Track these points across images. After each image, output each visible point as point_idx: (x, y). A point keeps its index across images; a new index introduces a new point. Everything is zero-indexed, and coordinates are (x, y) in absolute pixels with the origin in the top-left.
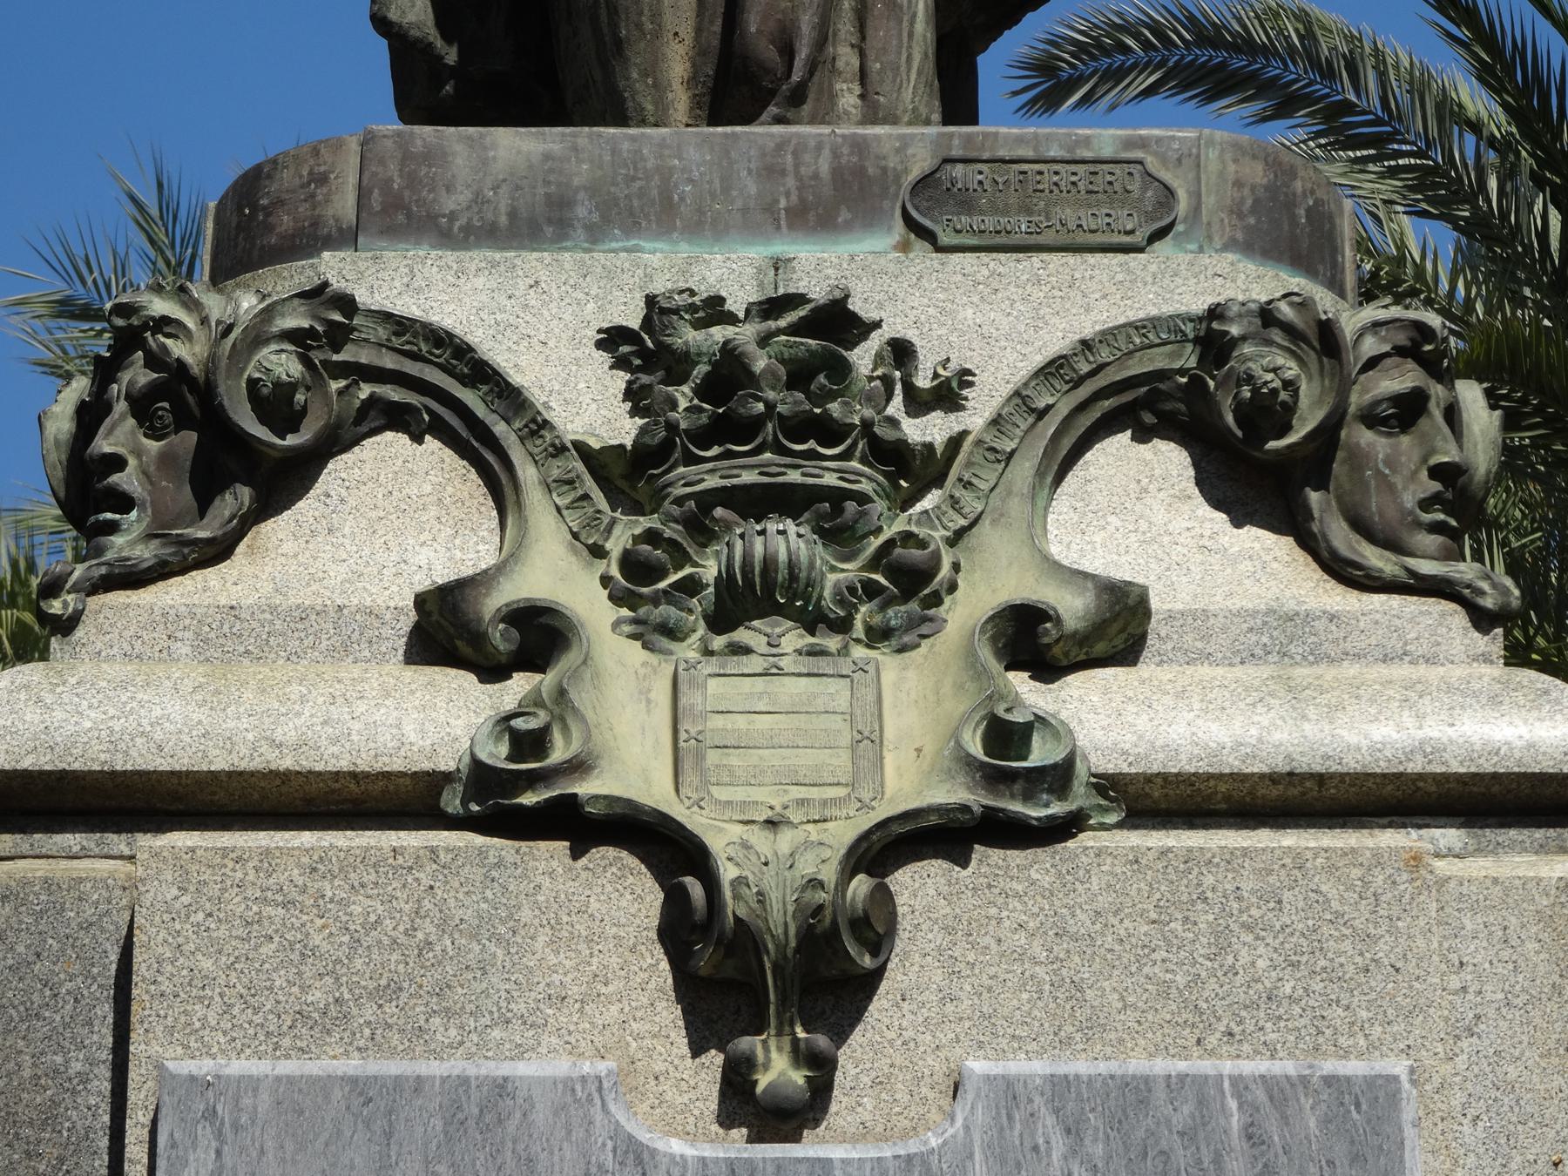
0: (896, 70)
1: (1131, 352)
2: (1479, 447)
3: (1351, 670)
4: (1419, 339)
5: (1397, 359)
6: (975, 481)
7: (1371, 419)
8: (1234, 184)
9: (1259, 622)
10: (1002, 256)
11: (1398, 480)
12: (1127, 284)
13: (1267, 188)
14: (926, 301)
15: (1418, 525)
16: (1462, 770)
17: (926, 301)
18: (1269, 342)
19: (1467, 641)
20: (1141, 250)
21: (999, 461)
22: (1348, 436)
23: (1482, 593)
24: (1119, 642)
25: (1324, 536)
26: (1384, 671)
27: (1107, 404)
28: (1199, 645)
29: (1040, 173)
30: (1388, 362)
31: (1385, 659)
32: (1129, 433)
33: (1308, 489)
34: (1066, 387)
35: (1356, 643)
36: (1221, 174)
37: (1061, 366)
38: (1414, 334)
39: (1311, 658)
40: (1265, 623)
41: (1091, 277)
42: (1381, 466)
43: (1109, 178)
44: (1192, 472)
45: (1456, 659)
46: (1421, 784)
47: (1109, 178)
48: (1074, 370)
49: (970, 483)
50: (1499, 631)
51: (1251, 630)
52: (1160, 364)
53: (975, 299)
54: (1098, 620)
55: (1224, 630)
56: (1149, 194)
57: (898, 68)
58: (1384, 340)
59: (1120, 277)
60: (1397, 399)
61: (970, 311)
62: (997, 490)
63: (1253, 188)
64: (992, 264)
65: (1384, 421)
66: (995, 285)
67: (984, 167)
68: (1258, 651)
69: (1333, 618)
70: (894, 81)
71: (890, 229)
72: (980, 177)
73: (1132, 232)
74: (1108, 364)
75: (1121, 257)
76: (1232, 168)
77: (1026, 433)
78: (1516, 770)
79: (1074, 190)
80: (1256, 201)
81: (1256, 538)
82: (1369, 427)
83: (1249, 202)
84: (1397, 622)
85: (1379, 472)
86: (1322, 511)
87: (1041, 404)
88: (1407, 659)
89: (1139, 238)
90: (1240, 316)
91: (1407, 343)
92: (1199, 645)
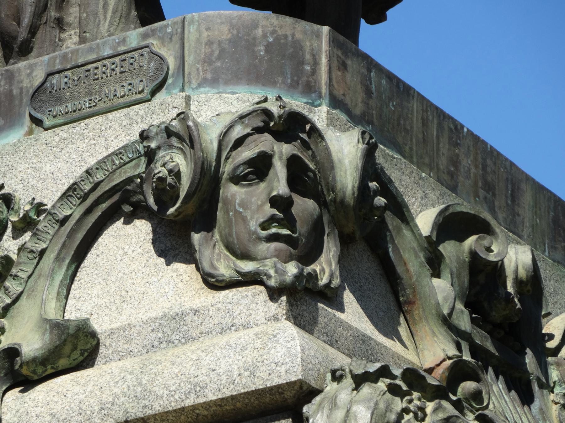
0: (96, 14)
1: (114, 171)
2: (348, 173)
3: (206, 342)
4: (268, 120)
5: (256, 136)
6: (19, 274)
7: (236, 179)
8: (206, 44)
9: (157, 324)
10: (65, 127)
11: (248, 214)
12: (128, 126)
13: (230, 41)
14: (27, 165)
15: (259, 239)
16: (214, 398)
17: (27, 165)
18: (171, 147)
19: (265, 310)
20: (149, 100)
21: (35, 258)
22: (223, 193)
23: (269, 277)
24: (77, 356)
25: (200, 260)
26: (223, 340)
27: (104, 206)
28: (126, 346)
29: (97, 68)
30: (250, 138)
31: (223, 331)
32: (122, 220)
33: (193, 233)
34: (79, 202)
35: (209, 324)
36: (198, 40)
37: (75, 190)
38: (264, 117)
39: (183, 341)
40: (160, 324)
41: (110, 127)
42: (237, 207)
43: (131, 61)
44: (151, 236)
45: (259, 323)
46: (197, 411)
47: (131, 61)
48: (82, 190)
49: (16, 276)
50: (284, 298)
51: (153, 330)
52: (129, 174)
53: (51, 158)
54: (52, 347)
55: (139, 334)
56: (152, 65)
57: (97, 14)
58: (247, 126)
59: (124, 123)
60: (250, 162)
61: (48, 165)
62: (33, 276)
63: (220, 43)
64: (61, 134)
65: (245, 178)
66: (62, 146)
67: (68, 73)
68: (156, 343)
69: (196, 312)
70: (95, 21)
71: (23, 124)
72: (66, 80)
73: (142, 91)
74: (102, 181)
75: (126, 110)
76: (205, 34)
77: (53, 236)
78: (243, 391)
79: (104, 76)
80: (222, 51)
81: (179, 266)
82: (236, 184)
83: (217, 53)
84: (230, 306)
85: (236, 211)
86: (200, 245)
87: (61, 216)
88: (233, 328)
89: (146, 94)
90: (157, 134)
91: (261, 124)
92: (126, 346)
